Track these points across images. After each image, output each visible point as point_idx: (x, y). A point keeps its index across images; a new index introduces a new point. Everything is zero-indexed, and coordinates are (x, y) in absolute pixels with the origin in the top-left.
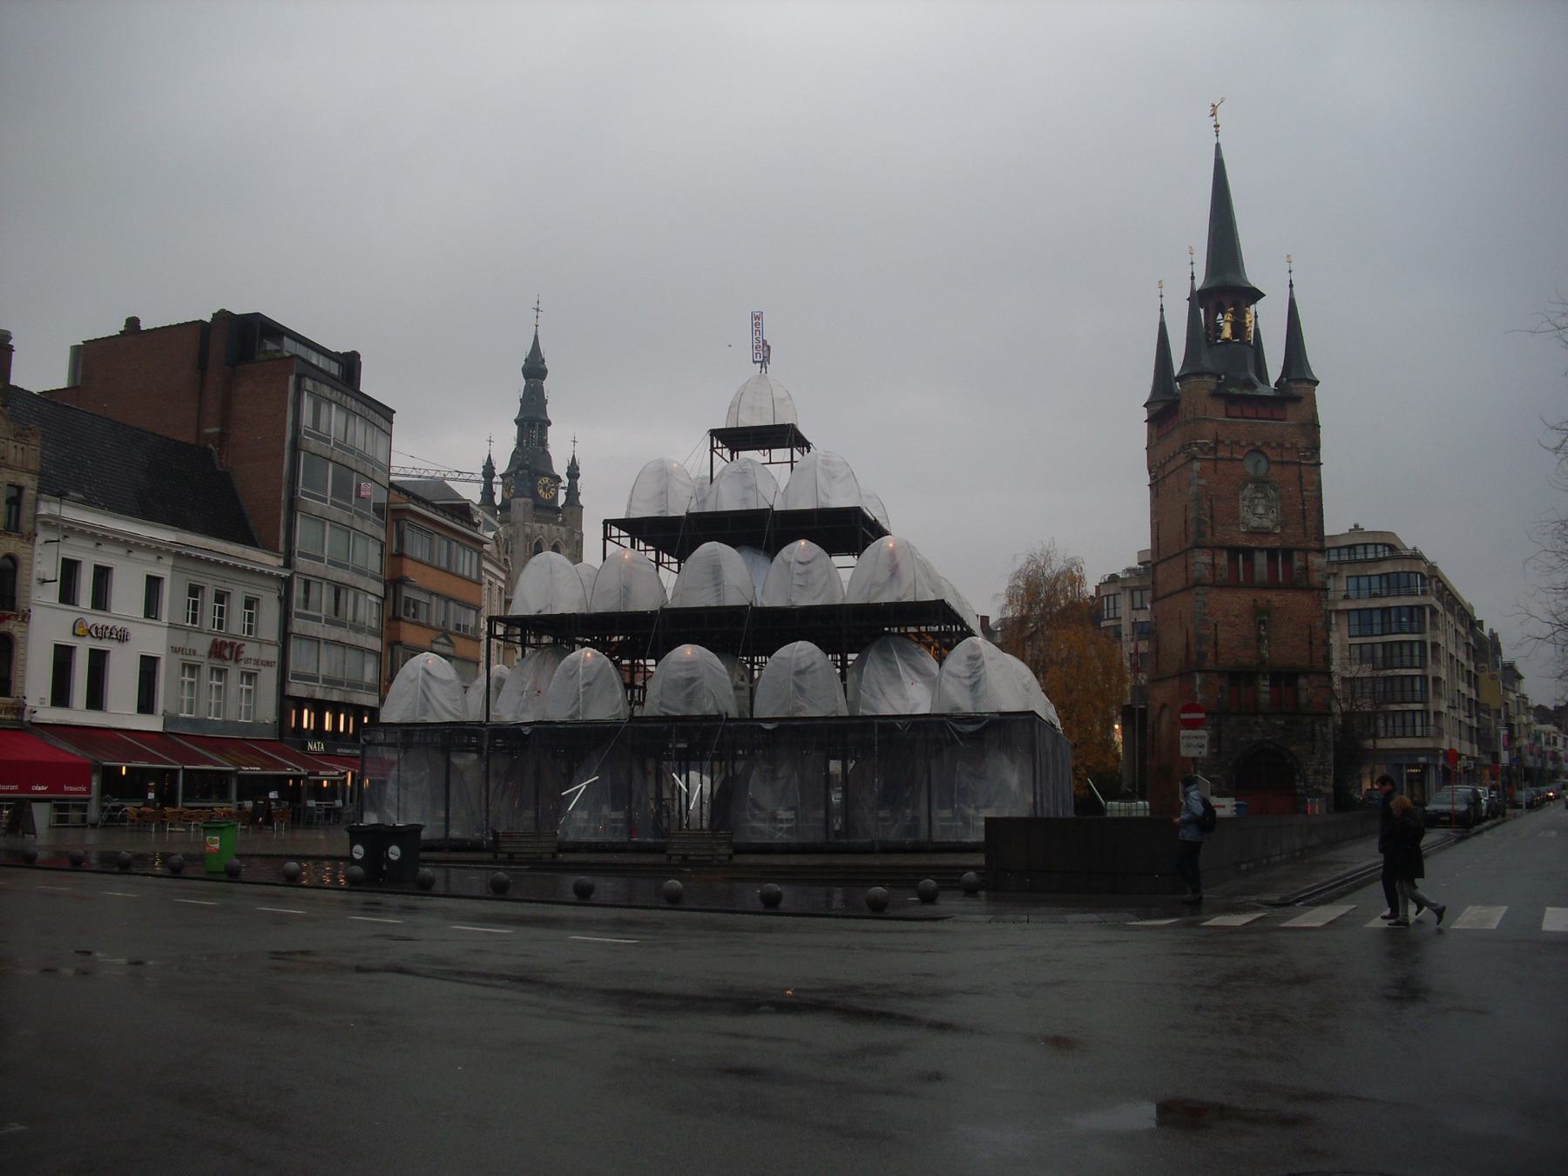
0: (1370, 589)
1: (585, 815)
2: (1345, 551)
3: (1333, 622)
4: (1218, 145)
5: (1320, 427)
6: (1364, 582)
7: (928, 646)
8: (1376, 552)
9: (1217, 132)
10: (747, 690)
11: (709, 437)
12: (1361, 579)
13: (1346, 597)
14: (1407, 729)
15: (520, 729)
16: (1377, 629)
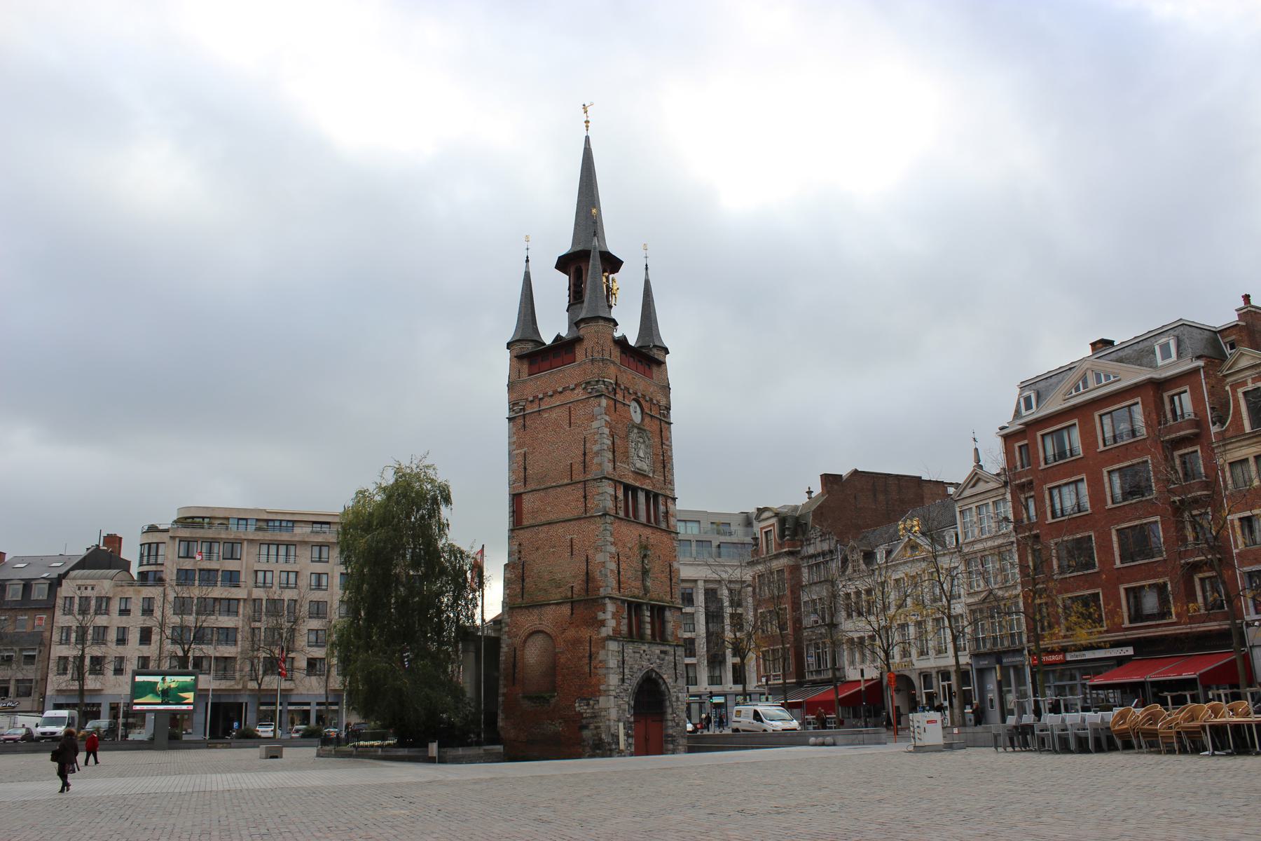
1: (1225, 535)
4: (587, 139)
7: (352, 623)
9: (587, 127)
10: (677, 655)
14: (1060, 508)
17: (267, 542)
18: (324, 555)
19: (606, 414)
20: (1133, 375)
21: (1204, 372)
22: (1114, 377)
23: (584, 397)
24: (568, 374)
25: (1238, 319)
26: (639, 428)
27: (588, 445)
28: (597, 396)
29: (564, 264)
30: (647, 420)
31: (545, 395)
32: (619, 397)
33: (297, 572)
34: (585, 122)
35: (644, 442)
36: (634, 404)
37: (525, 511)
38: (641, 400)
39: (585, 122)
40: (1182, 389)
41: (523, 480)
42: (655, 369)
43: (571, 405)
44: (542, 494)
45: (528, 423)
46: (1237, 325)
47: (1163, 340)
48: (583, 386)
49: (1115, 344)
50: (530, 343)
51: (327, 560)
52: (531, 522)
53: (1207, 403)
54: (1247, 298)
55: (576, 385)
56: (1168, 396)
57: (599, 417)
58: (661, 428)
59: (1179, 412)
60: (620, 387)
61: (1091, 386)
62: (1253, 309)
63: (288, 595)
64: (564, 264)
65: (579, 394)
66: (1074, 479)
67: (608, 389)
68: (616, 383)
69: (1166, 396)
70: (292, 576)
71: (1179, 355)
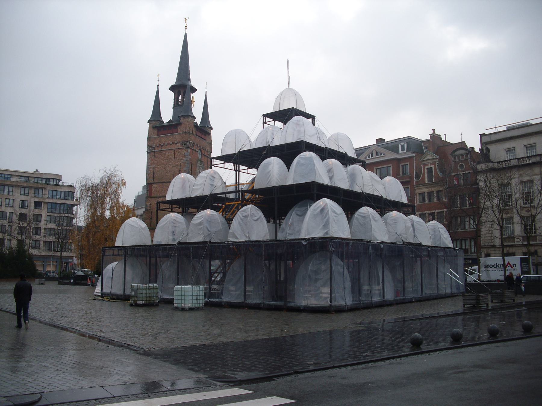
0: (57, 196)
2: (45, 180)
3: (43, 206)
4: (186, 34)
5: (212, 144)
6: (55, 193)
8: (53, 182)
9: (186, 29)
11: (262, 118)
12: (54, 192)
13: (48, 198)
15: (380, 245)
16: (58, 211)
17: (4, 185)
18: (27, 192)
19: (189, 155)
20: (391, 156)
21: (415, 158)
22: (383, 155)
23: (181, 148)
24: (176, 137)
25: (430, 138)
26: (200, 161)
27: (181, 167)
28: (186, 148)
29: (172, 88)
30: (203, 157)
31: (164, 144)
32: (194, 148)
33: (13, 200)
34: (185, 26)
35: (202, 166)
36: (199, 151)
37: (153, 191)
38: (202, 149)
39: (185, 26)
40: (407, 163)
41: (152, 178)
42: (207, 136)
43: (175, 150)
44: (161, 185)
45: (156, 155)
46: (429, 140)
47: (402, 143)
48: (181, 143)
49: (386, 141)
50: (158, 122)
51: (27, 194)
52: (156, 195)
53: (414, 170)
54: (434, 130)
55: (178, 142)
56: (402, 165)
57: (187, 157)
58: (208, 161)
59: (404, 172)
60: (195, 144)
61: (374, 157)
62: (435, 135)
63: (9, 210)
64: (172, 88)
65: (178, 146)
66: (387, 166)
67: (191, 145)
68: (194, 143)
69: (401, 165)
70: (11, 201)
71: (408, 150)
